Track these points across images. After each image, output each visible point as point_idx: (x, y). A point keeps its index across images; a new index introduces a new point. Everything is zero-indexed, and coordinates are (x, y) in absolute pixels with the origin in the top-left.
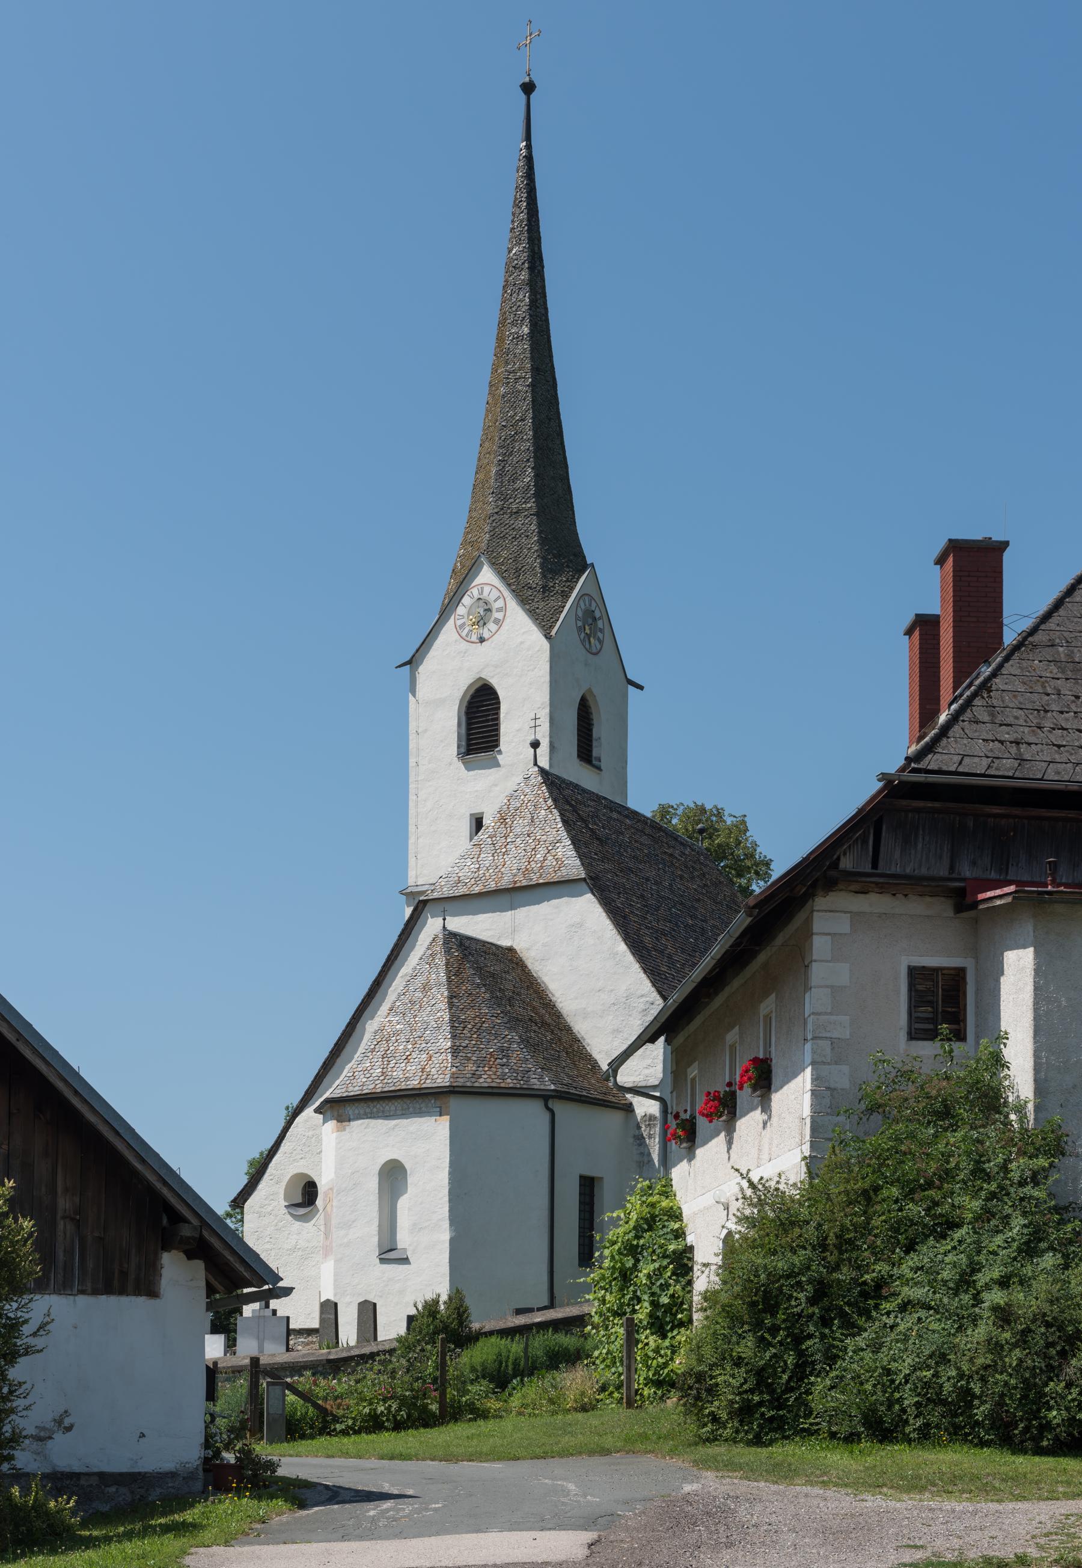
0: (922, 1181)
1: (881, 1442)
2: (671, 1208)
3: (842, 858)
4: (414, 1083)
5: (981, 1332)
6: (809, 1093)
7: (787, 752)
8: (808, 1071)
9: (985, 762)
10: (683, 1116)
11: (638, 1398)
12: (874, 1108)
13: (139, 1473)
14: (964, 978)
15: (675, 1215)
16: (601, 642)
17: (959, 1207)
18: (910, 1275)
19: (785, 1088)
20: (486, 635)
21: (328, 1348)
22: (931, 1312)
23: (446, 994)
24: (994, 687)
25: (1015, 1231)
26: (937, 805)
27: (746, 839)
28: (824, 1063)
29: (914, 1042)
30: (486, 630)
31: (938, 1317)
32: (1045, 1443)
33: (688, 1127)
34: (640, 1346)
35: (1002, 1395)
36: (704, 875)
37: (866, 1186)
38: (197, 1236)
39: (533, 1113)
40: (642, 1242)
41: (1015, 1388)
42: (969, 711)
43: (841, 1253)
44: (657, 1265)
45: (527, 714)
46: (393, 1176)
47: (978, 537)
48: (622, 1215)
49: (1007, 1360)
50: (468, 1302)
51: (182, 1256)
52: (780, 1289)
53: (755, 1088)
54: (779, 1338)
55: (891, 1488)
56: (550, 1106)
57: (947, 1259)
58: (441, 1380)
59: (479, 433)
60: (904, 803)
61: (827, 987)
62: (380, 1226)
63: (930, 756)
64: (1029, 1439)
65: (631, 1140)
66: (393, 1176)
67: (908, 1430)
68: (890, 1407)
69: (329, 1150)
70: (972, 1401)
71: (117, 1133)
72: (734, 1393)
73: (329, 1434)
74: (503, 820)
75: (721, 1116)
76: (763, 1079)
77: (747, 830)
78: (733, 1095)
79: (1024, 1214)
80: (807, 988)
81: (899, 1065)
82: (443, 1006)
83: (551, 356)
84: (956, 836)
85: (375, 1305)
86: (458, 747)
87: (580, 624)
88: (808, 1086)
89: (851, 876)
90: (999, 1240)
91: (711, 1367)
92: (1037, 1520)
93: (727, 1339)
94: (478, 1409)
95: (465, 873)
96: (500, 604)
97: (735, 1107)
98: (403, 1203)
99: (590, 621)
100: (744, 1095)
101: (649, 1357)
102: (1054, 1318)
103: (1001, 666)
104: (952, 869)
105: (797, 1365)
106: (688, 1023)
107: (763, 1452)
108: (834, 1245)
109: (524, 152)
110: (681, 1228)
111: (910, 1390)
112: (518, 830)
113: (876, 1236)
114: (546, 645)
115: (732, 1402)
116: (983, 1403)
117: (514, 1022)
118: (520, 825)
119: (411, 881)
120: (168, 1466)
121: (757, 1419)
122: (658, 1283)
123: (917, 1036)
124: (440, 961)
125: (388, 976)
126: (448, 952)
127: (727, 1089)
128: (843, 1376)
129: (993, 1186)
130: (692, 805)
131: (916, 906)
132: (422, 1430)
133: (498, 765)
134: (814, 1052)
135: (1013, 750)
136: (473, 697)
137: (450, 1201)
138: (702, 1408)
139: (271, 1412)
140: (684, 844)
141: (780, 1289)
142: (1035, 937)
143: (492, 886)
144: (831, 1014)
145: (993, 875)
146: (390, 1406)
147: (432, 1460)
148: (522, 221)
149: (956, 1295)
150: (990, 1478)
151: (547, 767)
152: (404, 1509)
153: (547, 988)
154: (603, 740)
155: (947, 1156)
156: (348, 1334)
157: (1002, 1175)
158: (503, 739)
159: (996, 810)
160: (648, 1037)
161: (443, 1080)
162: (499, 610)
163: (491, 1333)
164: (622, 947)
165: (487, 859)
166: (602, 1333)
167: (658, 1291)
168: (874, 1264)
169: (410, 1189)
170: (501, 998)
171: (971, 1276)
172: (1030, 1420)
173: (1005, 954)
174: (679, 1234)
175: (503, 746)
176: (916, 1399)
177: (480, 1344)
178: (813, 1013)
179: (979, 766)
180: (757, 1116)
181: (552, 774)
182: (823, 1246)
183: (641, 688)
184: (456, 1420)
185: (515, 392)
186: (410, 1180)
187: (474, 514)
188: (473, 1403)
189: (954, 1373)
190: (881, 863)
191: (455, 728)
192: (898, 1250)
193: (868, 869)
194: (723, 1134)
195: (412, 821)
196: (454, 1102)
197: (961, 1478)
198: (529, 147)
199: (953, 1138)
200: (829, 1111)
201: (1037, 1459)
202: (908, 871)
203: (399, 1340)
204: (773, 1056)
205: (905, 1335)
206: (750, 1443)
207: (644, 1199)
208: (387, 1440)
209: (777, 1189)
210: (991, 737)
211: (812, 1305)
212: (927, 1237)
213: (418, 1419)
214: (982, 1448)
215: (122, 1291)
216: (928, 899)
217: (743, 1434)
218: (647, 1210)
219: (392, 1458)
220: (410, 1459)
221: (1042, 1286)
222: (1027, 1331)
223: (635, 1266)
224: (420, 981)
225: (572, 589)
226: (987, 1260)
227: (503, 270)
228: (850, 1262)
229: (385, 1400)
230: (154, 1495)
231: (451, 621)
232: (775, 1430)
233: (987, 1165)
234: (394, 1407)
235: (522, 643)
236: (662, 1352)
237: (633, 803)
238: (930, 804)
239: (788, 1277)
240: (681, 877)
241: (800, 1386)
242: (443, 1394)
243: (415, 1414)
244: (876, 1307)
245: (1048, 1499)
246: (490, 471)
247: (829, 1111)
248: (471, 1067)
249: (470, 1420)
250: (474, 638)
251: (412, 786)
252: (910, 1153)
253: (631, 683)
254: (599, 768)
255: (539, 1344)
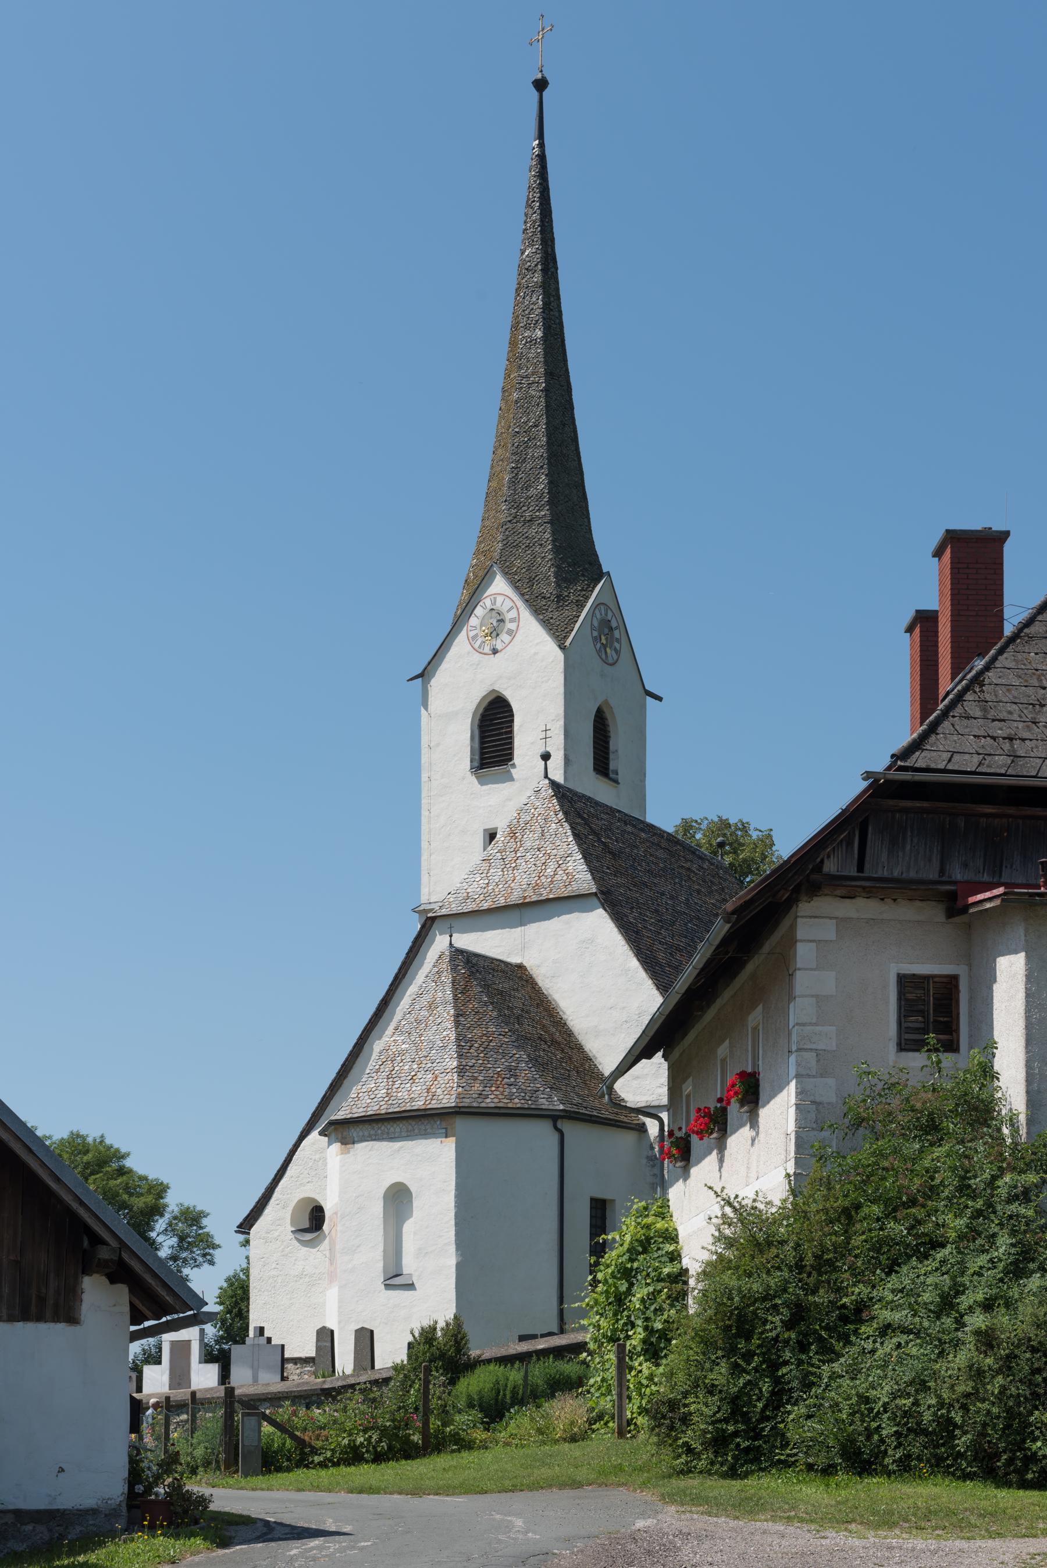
0: (904, 1199)
1: (860, 1474)
2: (667, 1230)
3: (826, 861)
4: (419, 1104)
5: (961, 1359)
6: (794, 1108)
7: (774, 755)
8: (793, 1085)
9: (976, 759)
10: (678, 1134)
11: (632, 1427)
12: (859, 1122)
13: (58, 1510)
14: (957, 987)
15: (671, 1237)
16: (618, 652)
17: (943, 1226)
18: (891, 1299)
19: (772, 1102)
20: (499, 647)
21: (324, 1376)
22: (911, 1337)
23: (452, 1012)
24: (987, 681)
25: (1001, 1250)
26: (925, 804)
27: (772, 854)
28: (809, 1076)
29: (904, 1054)
30: (499, 641)
31: (918, 1341)
32: (1030, 1476)
33: (682, 1145)
34: (633, 1373)
35: (985, 1425)
36: (723, 889)
37: (847, 1204)
38: (116, 1258)
39: (542, 1134)
40: (635, 1265)
41: (998, 1417)
42: (959, 706)
43: (820, 1274)
44: (651, 1289)
45: (541, 726)
46: (398, 1199)
47: (978, 527)
48: (617, 1238)
49: (989, 1387)
50: (466, 1328)
51: (104, 1280)
52: (754, 1313)
53: (742, 1103)
54: (754, 1365)
55: (861, 1523)
56: (559, 1126)
57: (929, 1281)
58: (430, 1409)
59: (491, 440)
60: (891, 802)
61: (812, 996)
62: (384, 1251)
63: (917, 753)
64: (1014, 1471)
65: (644, 1161)
66: (398, 1199)
67: (887, 1461)
68: (869, 1438)
69: (336, 1173)
70: (953, 1431)
71: (30, 1151)
72: (707, 1423)
73: (307, 1466)
74: (513, 834)
75: (712, 1133)
76: (751, 1093)
77: (773, 844)
78: (724, 1111)
79: (1013, 1233)
80: (791, 998)
81: (886, 1077)
82: (450, 1024)
83: (565, 360)
84: (944, 838)
85: (372, 1332)
86: (471, 761)
87: (595, 634)
88: (793, 1100)
89: (836, 880)
90: (983, 1260)
91: (686, 1394)
92: (1000, 1560)
93: (700, 1365)
94: (463, 1440)
95: (474, 889)
96: (513, 614)
97: (726, 1123)
98: (408, 1227)
99: (606, 631)
100: (734, 1109)
101: (642, 1385)
102: (1040, 1342)
103: (994, 659)
104: (942, 872)
105: (773, 1393)
106: (683, 1039)
107: (737, 1484)
108: (812, 1266)
109: (537, 151)
110: (676, 1250)
111: (889, 1419)
112: (528, 844)
113: (856, 1257)
114: (560, 655)
115: (705, 1432)
116: (965, 1433)
117: (522, 1041)
118: (530, 840)
119: (424, 899)
120: (89, 1503)
121: (732, 1450)
122: (652, 1308)
123: (907, 1047)
124: (447, 978)
125: (396, 995)
126: (454, 969)
127: (719, 1105)
128: (821, 1405)
129: (979, 1204)
130: (716, 819)
131: (905, 911)
132: (403, 1462)
133: (512, 779)
134: (798, 1064)
135: (1006, 746)
136: (486, 709)
137: (456, 1224)
138: (677, 1439)
139: (246, 1443)
140: (702, 858)
141: (754, 1313)
142: (1026, 941)
143: (502, 902)
144: (816, 1024)
145: (986, 878)
146: (370, 1437)
147: (400, 1493)
148: (535, 222)
149: (938, 1318)
150: (968, 1513)
151: (559, 778)
152: (329, 1547)
153: (558, 1005)
154: (620, 752)
155: (932, 1172)
156: (345, 1361)
157: (989, 1191)
158: (517, 753)
159: (989, 809)
160: (642, 1051)
161: (447, 1100)
162: (512, 620)
163: (489, 1361)
164: (634, 963)
165: (496, 874)
166: (597, 1360)
167: (652, 1315)
168: (854, 1285)
169: (416, 1212)
170: (509, 1017)
171: (955, 1297)
172: (1014, 1452)
173: (998, 960)
174: (675, 1257)
175: (517, 759)
176: (895, 1429)
177: (478, 1371)
178: (797, 1024)
179: (970, 763)
180: (746, 1132)
181: (570, 790)
182: (799, 1267)
183: (660, 699)
184: (439, 1452)
185: (528, 398)
186: (415, 1204)
187: (487, 523)
188: (458, 1434)
189: (933, 1401)
190: (867, 866)
191: (468, 742)
192: (878, 1272)
193: (853, 872)
194: (715, 1152)
195: (424, 837)
196: (460, 1123)
197: (936, 1513)
198: (541, 145)
199: (938, 1152)
200: (814, 1126)
201: (1021, 1493)
202: (896, 874)
203: (396, 1368)
204: (761, 1070)
205: (885, 1361)
206: (724, 1476)
207: (639, 1220)
208: (365, 1473)
209: (754, 1208)
210: (982, 733)
211: (788, 1330)
212: (909, 1257)
213: (401, 1450)
214: (964, 1481)
215: (40, 1318)
216: (918, 903)
217: (718, 1466)
218: (642, 1232)
219: (360, 1492)
220: (378, 1493)
221: (1027, 1310)
222: (1011, 1357)
223: (629, 1289)
224: (424, 1001)
225: (587, 598)
226: (971, 1281)
227: (516, 272)
228: (829, 1283)
229: (365, 1431)
230: (75, 1532)
231: (464, 633)
232: (752, 1462)
233: (973, 1181)
234: (375, 1437)
235: (536, 654)
236: (656, 1380)
237: (650, 819)
238: (918, 804)
239: (764, 1299)
240: (699, 892)
241: (777, 1415)
242: (426, 1423)
243: (396, 1446)
244: (856, 1332)
245: (1024, 1536)
246: (503, 479)
247: (814, 1126)
248: (477, 1087)
249: (453, 1451)
250: (487, 649)
251: (424, 801)
252: (893, 1169)
253: (649, 694)
254: (616, 782)
255: (538, 1372)
